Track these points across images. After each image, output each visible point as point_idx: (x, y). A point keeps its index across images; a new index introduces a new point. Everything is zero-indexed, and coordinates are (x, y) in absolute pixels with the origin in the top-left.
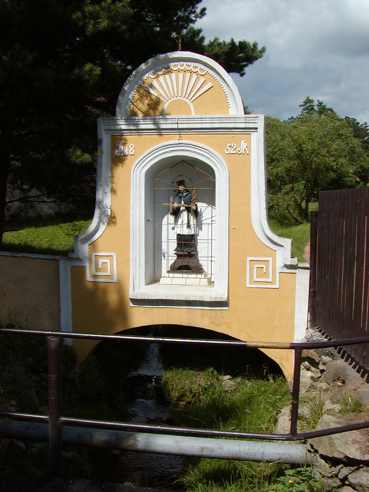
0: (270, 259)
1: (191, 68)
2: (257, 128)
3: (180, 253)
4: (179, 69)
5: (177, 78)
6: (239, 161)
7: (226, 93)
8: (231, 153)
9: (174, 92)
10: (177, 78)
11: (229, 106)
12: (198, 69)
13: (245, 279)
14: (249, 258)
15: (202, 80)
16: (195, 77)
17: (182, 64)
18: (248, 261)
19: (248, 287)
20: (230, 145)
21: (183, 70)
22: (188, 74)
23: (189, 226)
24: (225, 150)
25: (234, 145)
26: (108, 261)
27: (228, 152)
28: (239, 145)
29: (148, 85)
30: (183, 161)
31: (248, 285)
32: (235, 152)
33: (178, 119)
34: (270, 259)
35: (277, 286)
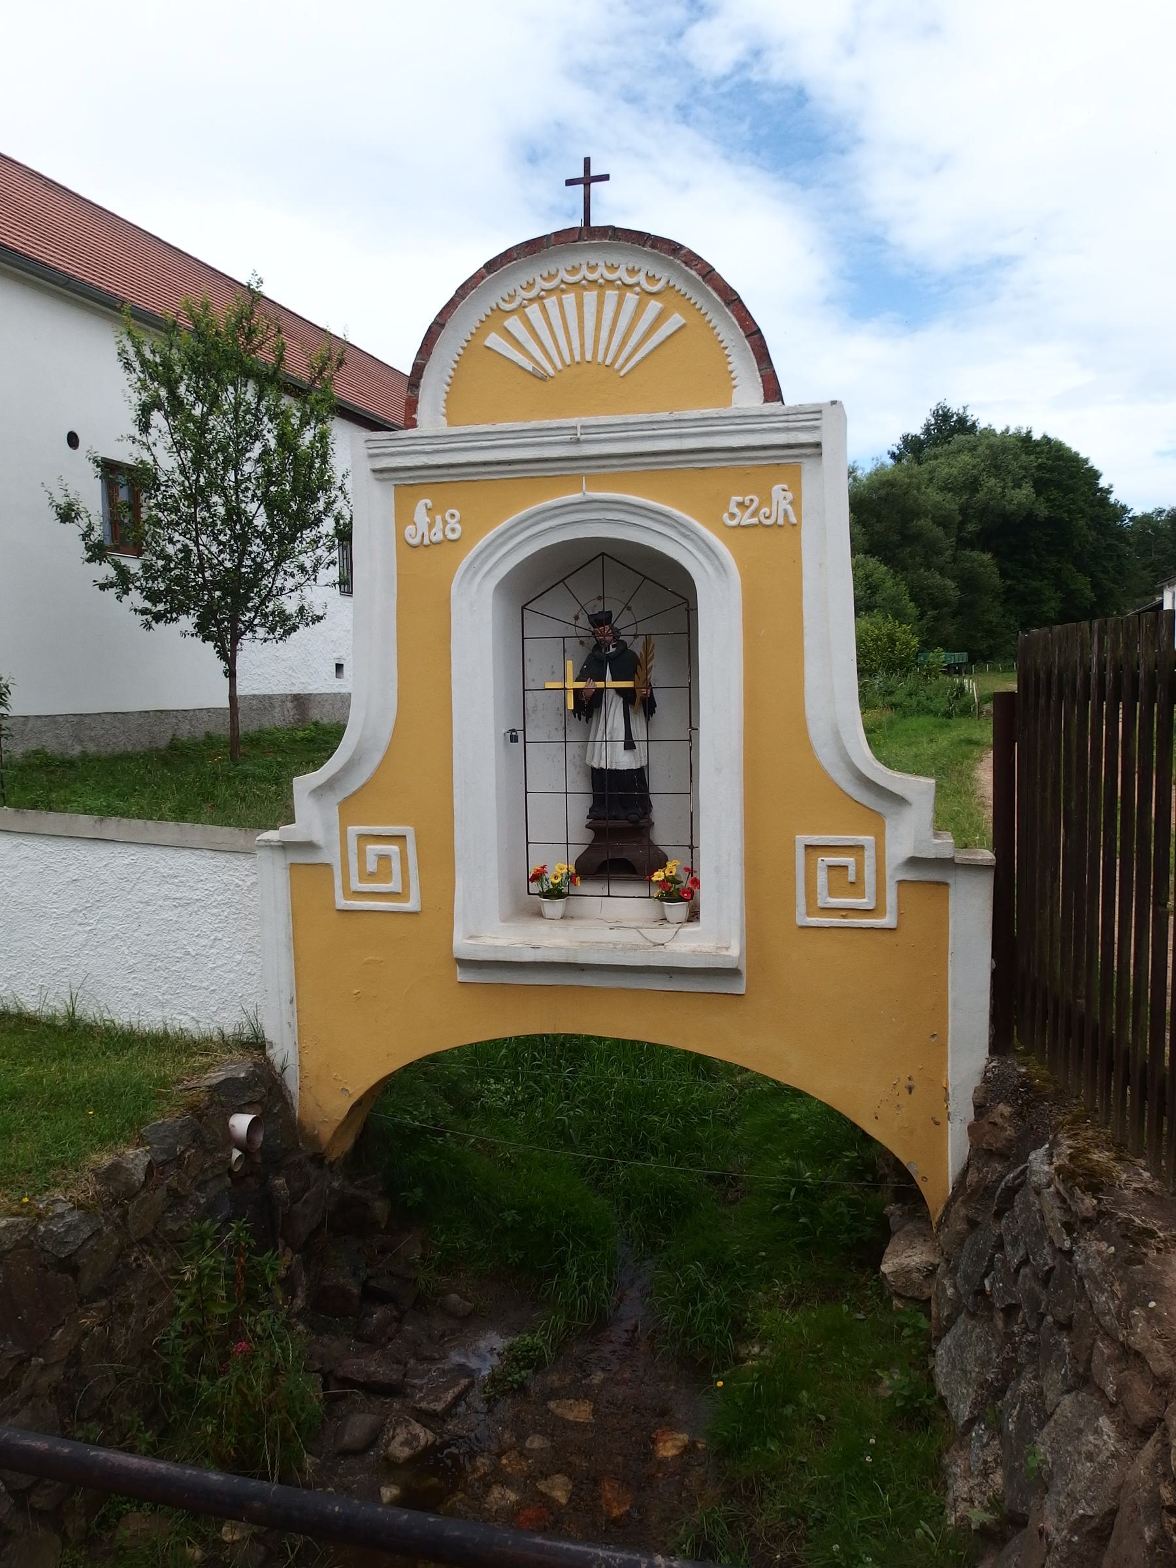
0: (867, 840)
1: (621, 273)
2: (818, 445)
3: (601, 823)
4: (584, 278)
5: (580, 306)
6: (772, 557)
7: (723, 345)
8: (743, 523)
9: (572, 356)
10: (580, 306)
11: (734, 383)
12: (641, 277)
13: (813, 831)
14: (803, 839)
15: (654, 306)
16: (631, 299)
17: (593, 263)
18: (800, 853)
19: (800, 923)
20: (740, 499)
21: (596, 281)
22: (611, 295)
23: (629, 745)
24: (726, 515)
25: (752, 500)
26: (393, 849)
27: (734, 523)
28: (767, 500)
29: (991, 1319)
30: (603, 554)
31: (342, 903)
32: (754, 520)
33: (582, 427)
34: (867, 840)
35: (412, 905)
